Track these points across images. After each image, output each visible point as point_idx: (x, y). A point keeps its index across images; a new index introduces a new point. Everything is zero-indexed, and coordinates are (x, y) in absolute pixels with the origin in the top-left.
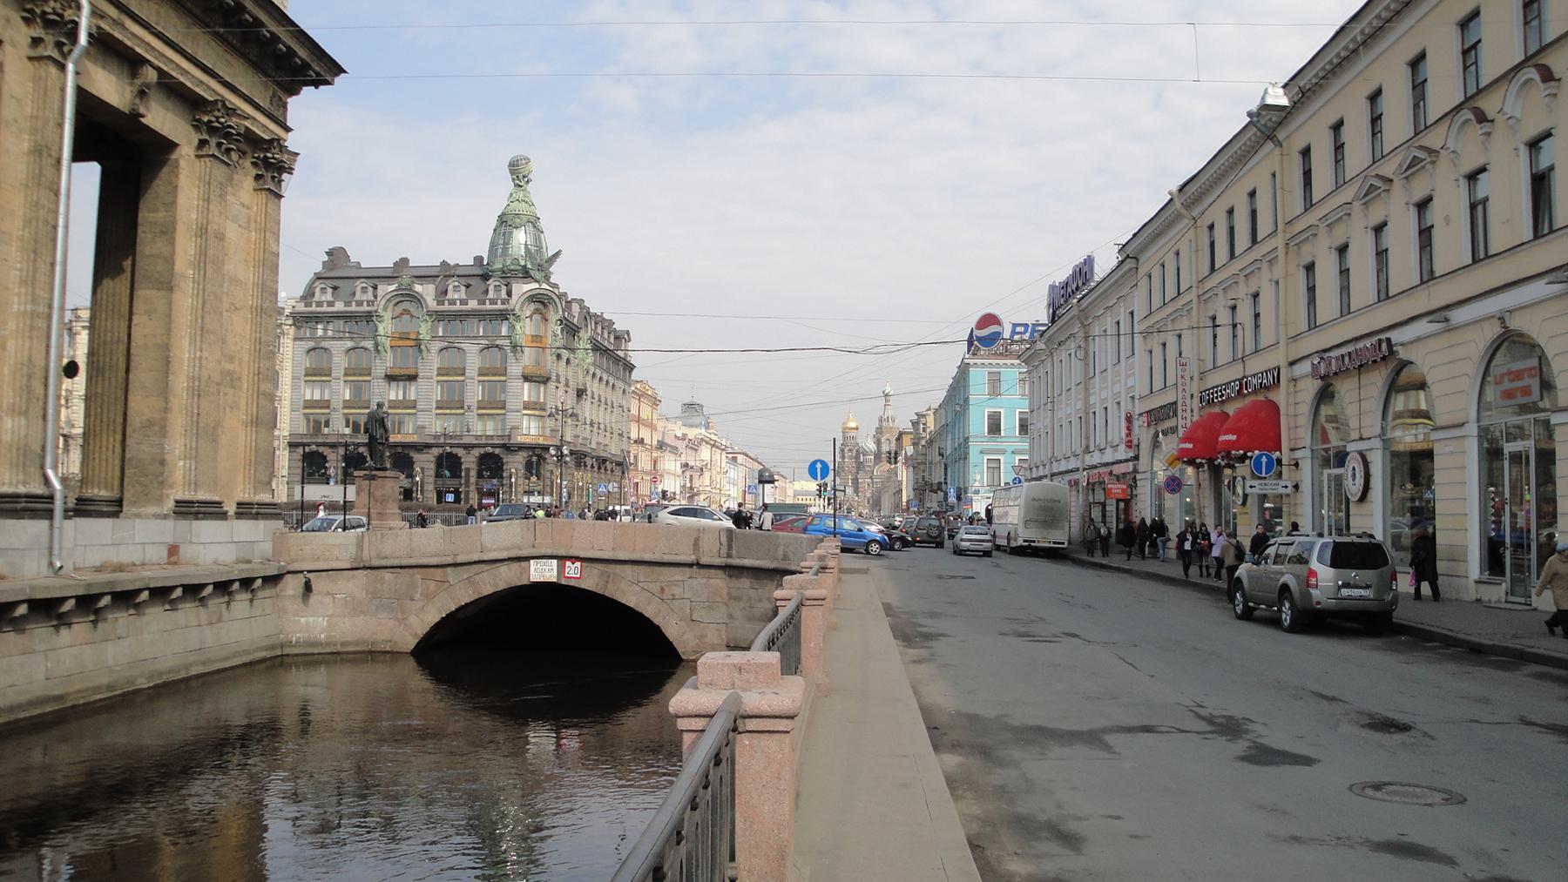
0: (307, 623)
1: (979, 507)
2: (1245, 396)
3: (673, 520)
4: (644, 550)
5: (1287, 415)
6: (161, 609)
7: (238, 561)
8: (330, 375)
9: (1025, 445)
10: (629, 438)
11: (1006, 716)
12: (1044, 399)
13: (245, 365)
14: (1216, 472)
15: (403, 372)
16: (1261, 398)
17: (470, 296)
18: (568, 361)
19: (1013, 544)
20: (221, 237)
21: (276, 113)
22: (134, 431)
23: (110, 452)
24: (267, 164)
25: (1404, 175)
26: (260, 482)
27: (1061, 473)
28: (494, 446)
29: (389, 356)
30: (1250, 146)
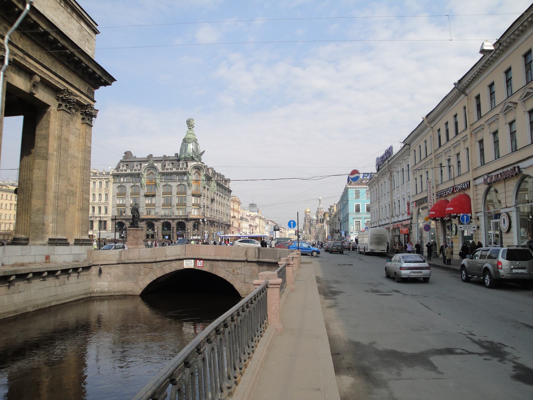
0: (100, 285)
1: (353, 238)
2: (455, 193)
3: (240, 244)
4: (226, 256)
5: (473, 199)
6: (39, 280)
7: (74, 261)
8: (125, 195)
9: (369, 216)
10: (230, 216)
11: (375, 343)
12: (375, 198)
13: (78, 188)
14: (443, 222)
15: (150, 194)
16: (462, 193)
17: (173, 167)
18: (208, 189)
19: (366, 251)
20: (67, 140)
21: (90, 95)
22: (33, 213)
23: (26, 221)
24: (86, 114)
25: (504, 113)
26: (83, 232)
27: (383, 225)
28: (182, 219)
29: (146, 188)
30: (454, 97)
